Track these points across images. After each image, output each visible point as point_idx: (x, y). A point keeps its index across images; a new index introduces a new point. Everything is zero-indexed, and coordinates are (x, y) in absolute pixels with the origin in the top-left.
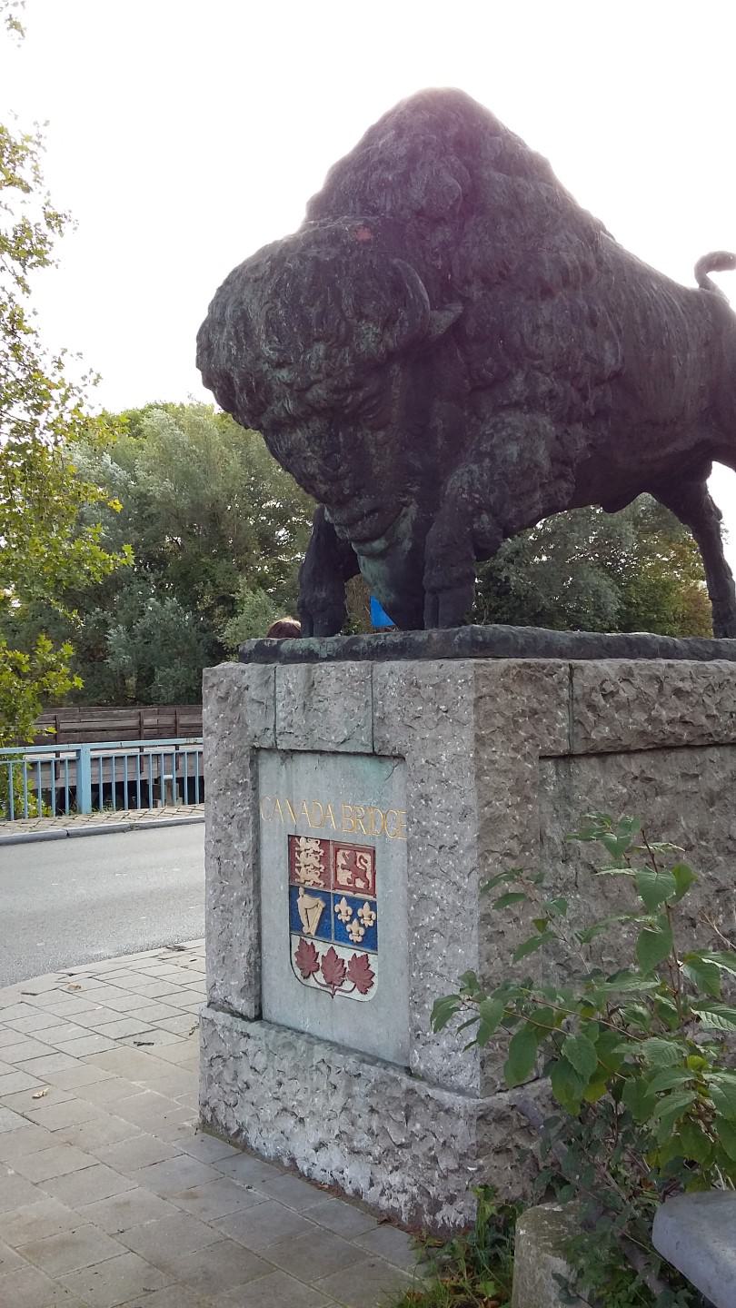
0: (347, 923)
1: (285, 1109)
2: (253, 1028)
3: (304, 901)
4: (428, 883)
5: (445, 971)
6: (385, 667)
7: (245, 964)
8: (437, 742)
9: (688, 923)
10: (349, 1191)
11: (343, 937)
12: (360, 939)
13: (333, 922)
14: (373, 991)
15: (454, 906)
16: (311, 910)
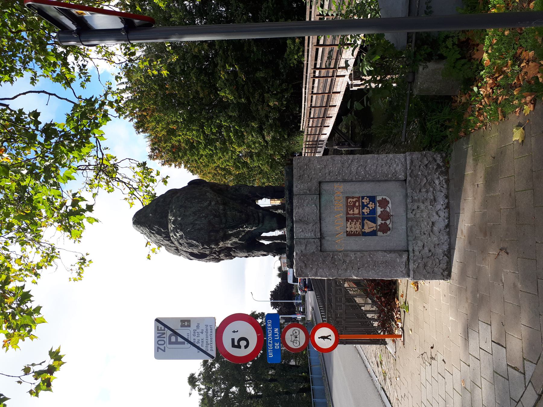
0: (369, 209)
1: (432, 231)
2: (411, 249)
3: (367, 230)
4: (353, 172)
5: (375, 165)
6: (295, 189)
7: (391, 254)
8: (315, 169)
9: (358, 173)
10: (446, 201)
11: (373, 211)
12: (373, 204)
13: (370, 216)
14: (388, 199)
15: (357, 162)
16: (369, 226)
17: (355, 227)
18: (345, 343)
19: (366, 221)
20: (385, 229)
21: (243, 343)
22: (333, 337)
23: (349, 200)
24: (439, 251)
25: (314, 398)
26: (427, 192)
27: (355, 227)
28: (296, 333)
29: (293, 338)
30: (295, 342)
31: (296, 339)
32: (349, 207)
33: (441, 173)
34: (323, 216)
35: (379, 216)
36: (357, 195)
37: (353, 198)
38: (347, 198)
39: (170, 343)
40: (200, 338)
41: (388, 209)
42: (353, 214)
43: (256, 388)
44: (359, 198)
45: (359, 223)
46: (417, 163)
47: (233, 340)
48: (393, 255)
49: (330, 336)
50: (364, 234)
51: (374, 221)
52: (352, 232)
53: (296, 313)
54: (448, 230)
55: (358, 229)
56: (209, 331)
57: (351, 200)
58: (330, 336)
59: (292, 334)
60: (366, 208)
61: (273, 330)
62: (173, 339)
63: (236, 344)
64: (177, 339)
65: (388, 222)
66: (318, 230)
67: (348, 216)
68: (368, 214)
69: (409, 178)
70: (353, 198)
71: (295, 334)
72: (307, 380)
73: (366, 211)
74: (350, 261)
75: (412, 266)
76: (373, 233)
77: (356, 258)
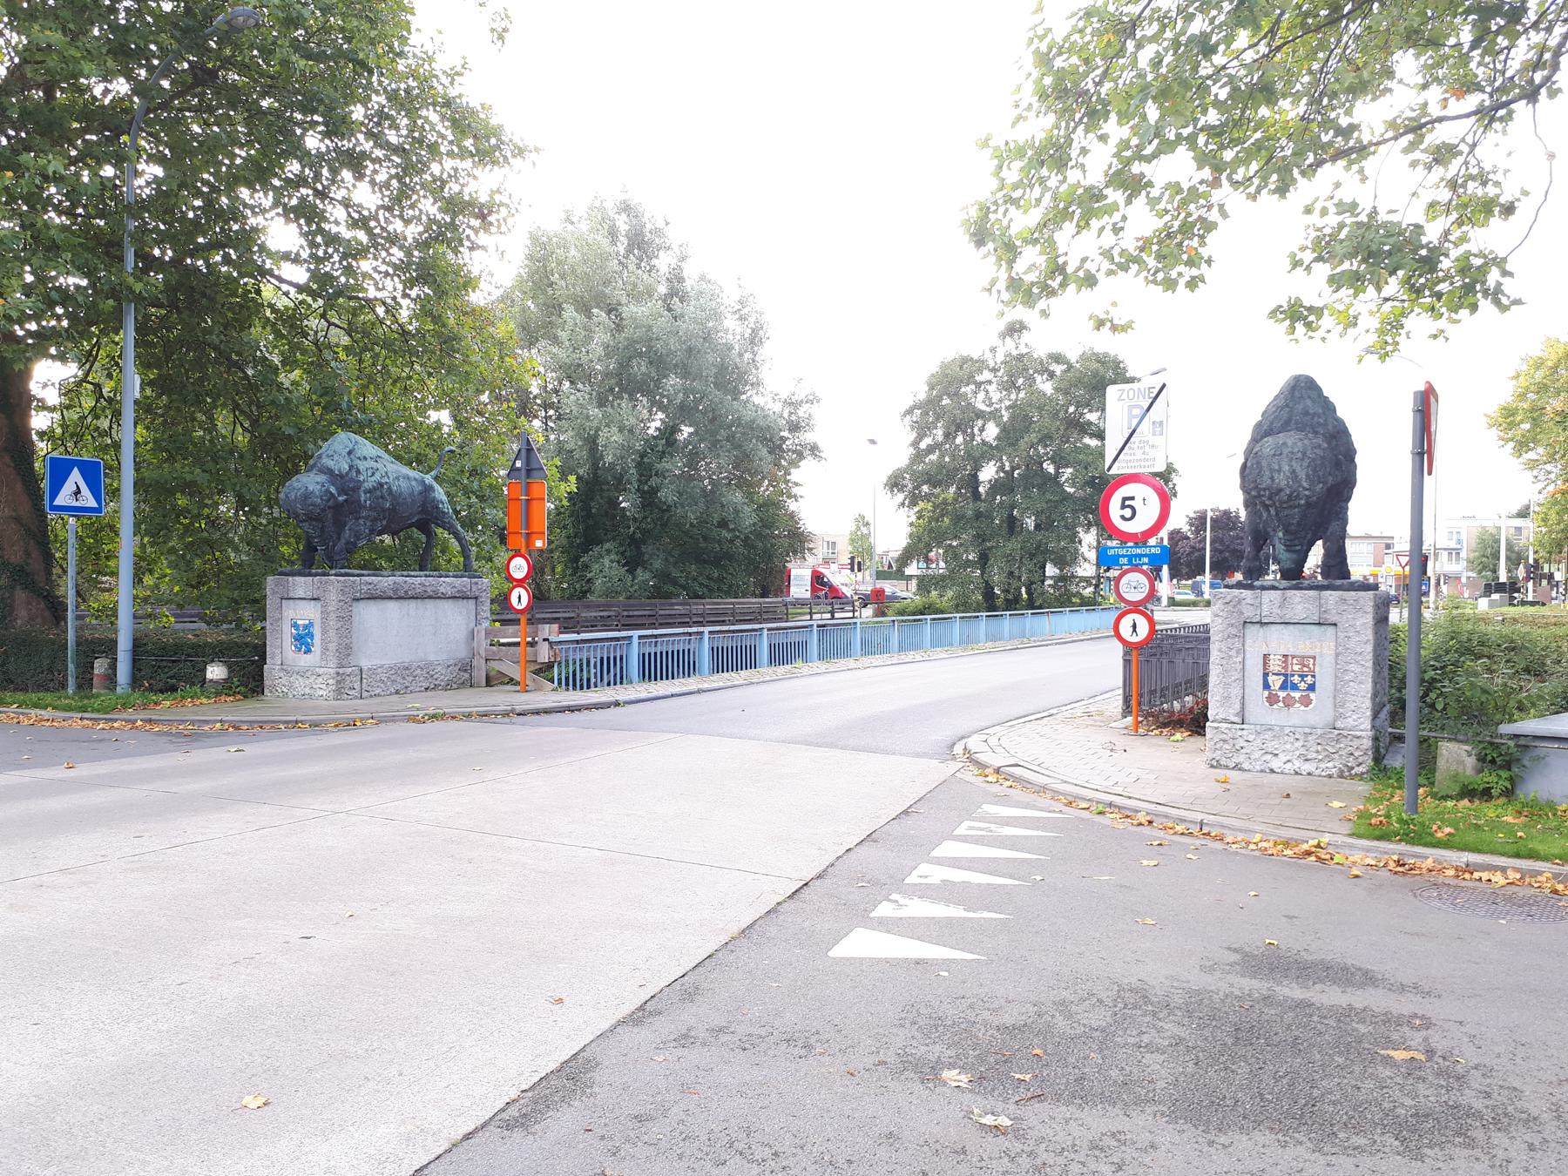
3: (1271, 678)
11: (1295, 687)
16: (1275, 682)
17: (1275, 664)
18: (1314, 394)
20: (1272, 700)
21: (1128, 513)
22: (1134, 639)
24: (1241, 758)
25: (769, 630)
26: (1317, 752)
27: (1275, 664)
29: (1134, 584)
32: (1303, 660)
33: (1342, 771)
34: (1291, 627)
38: (1314, 658)
39: (1131, 407)
40: (1136, 450)
41: (1297, 705)
43: (996, 487)
46: (1356, 743)
47: (1132, 498)
48: (1238, 706)
50: (1266, 675)
51: (1283, 687)
53: (1175, 581)
55: (1272, 668)
56: (1146, 463)
61: (1145, 555)
62: (1137, 412)
63: (1127, 503)
64: (1135, 417)
65: (1281, 704)
66: (1272, 620)
69: (1336, 732)
72: (1012, 603)
73: (1296, 679)
74: (1230, 656)
75: (1224, 725)
76: (1266, 686)
77: (1235, 663)
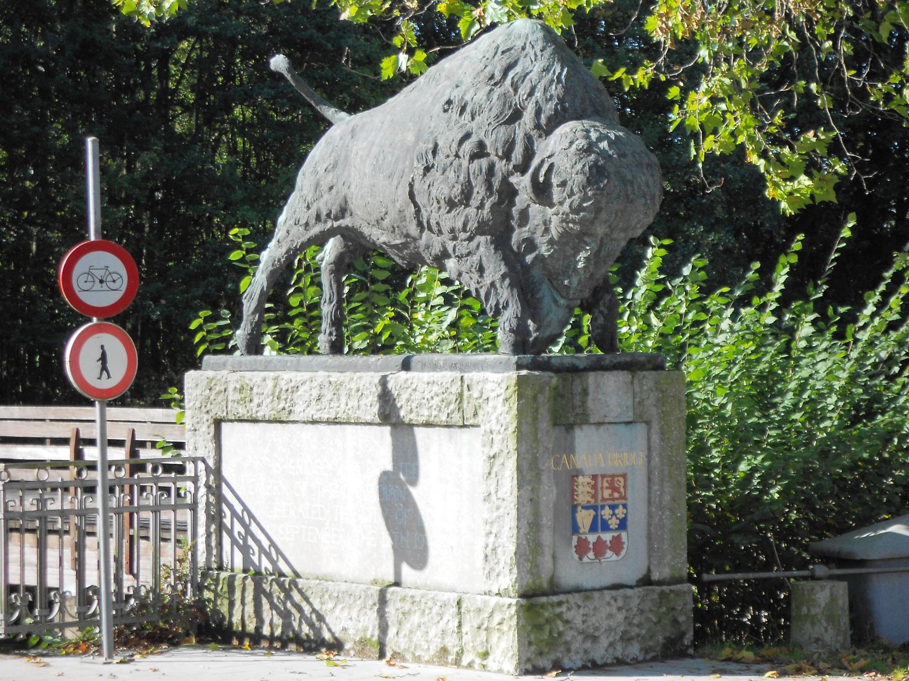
11: (606, 527)
14: (623, 553)
16: (584, 518)
19: (592, 512)
20: (582, 548)
23: (621, 479)
28: (114, 281)
29: (99, 274)
30: (90, 279)
31: (97, 281)
35: (599, 538)
36: (629, 495)
37: (625, 487)
38: (624, 476)
42: (602, 488)
44: (625, 498)
45: (589, 499)
49: (109, 377)
51: (593, 529)
52: (577, 486)
54: (589, 665)
57: (622, 484)
58: (109, 377)
59: (111, 270)
60: (611, 512)
67: (600, 479)
68: (602, 516)
70: (625, 487)
71: (109, 278)
73: (606, 513)
